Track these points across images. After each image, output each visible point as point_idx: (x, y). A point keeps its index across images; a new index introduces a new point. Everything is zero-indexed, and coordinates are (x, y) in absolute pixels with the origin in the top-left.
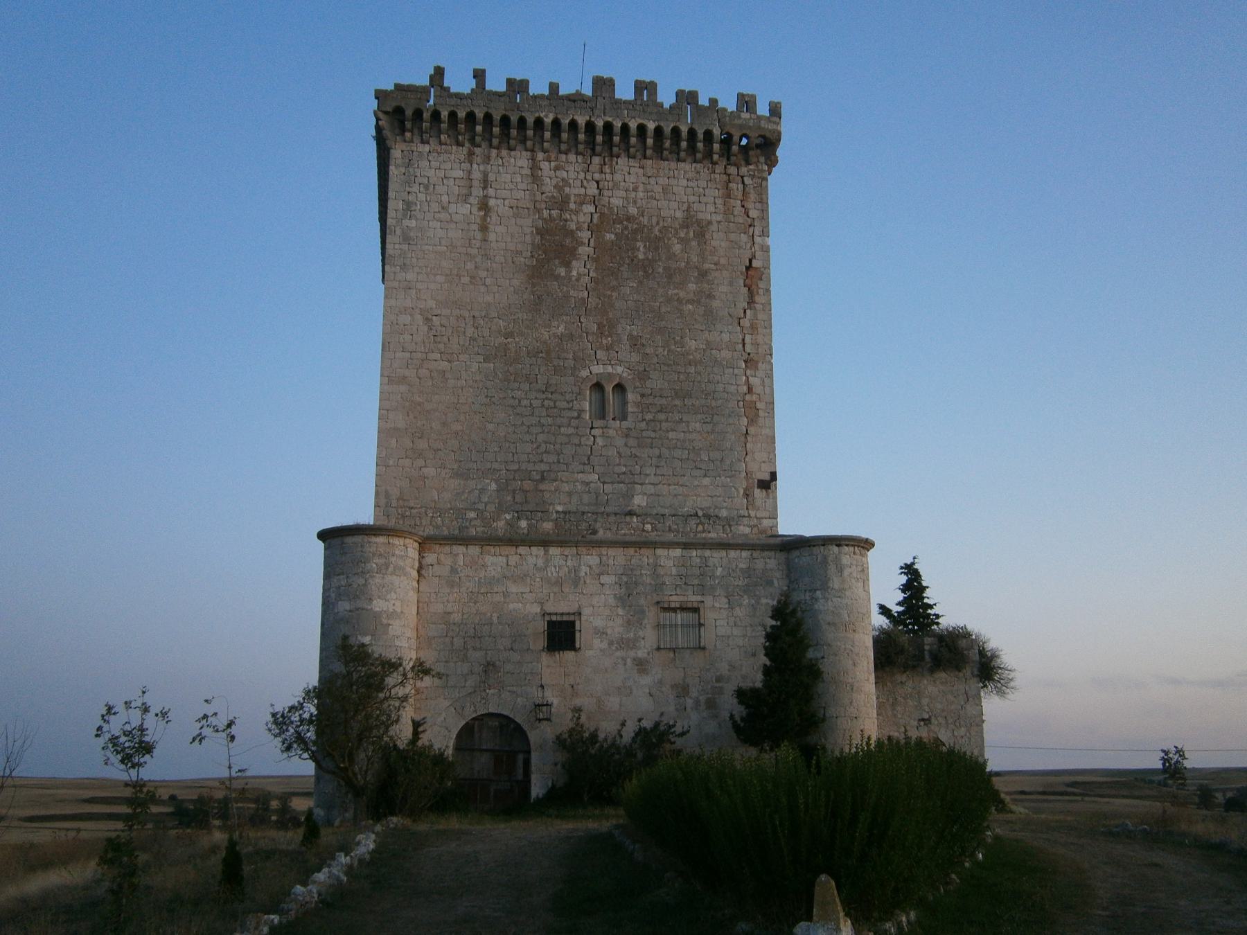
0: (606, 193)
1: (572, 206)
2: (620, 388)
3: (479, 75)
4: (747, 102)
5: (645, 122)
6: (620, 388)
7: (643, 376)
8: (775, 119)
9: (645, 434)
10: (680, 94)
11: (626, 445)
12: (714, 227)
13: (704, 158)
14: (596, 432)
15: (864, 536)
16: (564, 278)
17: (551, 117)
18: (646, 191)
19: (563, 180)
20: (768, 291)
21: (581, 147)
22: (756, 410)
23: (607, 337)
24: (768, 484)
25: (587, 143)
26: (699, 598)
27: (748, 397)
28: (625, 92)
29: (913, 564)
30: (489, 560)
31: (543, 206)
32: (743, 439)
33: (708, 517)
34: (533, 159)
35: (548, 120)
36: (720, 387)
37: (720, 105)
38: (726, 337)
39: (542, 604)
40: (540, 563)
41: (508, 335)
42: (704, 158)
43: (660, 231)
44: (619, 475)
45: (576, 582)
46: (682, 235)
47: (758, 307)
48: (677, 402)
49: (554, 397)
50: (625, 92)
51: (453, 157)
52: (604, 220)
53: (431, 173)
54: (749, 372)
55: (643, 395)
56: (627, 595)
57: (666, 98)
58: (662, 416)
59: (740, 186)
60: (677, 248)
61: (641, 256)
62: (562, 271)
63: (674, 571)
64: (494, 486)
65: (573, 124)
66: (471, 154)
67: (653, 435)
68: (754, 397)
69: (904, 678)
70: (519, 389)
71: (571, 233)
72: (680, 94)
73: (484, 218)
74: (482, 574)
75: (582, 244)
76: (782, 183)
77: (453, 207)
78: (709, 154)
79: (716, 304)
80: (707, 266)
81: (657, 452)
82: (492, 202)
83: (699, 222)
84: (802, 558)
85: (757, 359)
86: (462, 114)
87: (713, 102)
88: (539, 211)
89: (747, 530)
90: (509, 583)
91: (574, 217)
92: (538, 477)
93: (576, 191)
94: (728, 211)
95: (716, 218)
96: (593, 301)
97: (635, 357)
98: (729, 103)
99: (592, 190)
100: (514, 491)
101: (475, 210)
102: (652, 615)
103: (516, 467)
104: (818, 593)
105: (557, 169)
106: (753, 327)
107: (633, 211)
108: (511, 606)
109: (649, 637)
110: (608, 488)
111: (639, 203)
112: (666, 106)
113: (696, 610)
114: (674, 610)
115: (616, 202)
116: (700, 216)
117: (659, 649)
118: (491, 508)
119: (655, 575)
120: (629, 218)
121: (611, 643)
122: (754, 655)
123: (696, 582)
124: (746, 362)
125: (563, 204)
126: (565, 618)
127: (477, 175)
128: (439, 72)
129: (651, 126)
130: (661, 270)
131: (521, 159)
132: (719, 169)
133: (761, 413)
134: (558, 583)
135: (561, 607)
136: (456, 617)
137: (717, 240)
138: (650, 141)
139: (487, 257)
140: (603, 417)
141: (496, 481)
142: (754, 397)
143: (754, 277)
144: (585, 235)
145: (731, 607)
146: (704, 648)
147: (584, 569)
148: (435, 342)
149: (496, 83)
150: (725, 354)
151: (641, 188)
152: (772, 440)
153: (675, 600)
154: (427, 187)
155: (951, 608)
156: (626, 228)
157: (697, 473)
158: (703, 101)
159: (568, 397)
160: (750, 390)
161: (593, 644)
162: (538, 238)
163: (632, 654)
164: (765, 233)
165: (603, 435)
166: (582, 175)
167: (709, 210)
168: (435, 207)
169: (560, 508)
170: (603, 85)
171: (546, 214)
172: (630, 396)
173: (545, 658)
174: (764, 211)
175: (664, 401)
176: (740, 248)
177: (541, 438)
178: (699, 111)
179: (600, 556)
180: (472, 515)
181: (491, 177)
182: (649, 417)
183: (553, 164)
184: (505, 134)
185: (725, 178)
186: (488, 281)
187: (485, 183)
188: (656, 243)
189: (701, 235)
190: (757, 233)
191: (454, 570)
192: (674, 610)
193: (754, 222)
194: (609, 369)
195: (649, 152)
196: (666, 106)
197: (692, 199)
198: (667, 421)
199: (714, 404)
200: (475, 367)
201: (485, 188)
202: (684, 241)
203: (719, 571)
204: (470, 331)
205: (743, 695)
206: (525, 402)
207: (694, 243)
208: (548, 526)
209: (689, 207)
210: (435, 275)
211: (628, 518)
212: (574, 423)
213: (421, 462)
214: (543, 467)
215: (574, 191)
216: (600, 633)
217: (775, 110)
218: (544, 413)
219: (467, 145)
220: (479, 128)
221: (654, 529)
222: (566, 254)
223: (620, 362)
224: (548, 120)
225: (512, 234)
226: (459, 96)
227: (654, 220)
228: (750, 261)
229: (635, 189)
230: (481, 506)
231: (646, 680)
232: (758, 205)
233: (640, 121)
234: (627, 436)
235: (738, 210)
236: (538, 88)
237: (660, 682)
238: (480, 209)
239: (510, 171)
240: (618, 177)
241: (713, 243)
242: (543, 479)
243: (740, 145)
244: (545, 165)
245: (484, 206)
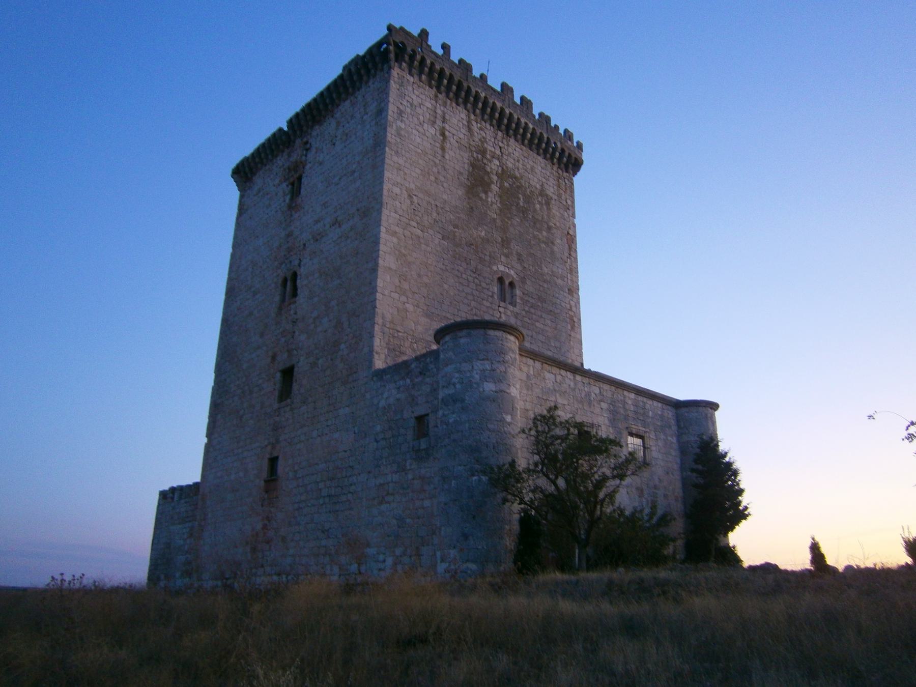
7: (523, 280)
62: (483, 196)
79: (555, 248)
144: (495, 178)
174: (573, 202)
175: (533, 301)
177: (473, 304)
179: (600, 388)
186: (445, 185)
188: (528, 199)
212: (490, 299)
244: (474, 123)
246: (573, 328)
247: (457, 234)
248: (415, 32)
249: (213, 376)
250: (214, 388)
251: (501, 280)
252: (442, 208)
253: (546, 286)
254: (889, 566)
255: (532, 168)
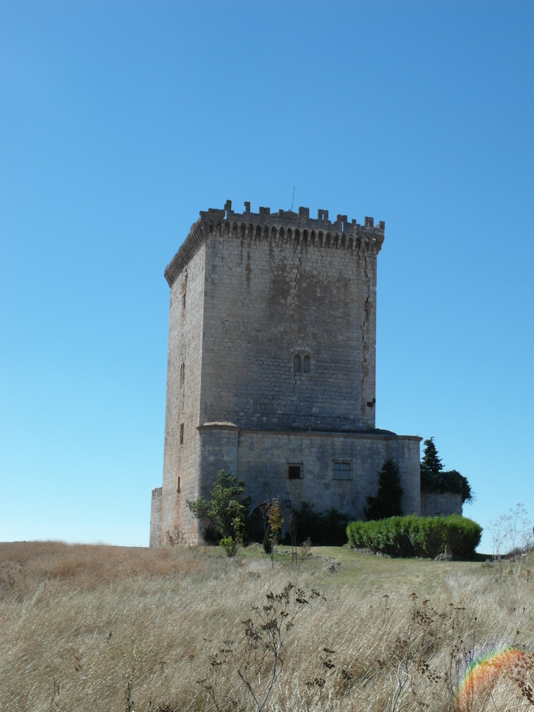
0: (303, 264)
1: (288, 270)
2: (307, 357)
3: (247, 205)
4: (369, 221)
5: (322, 230)
6: (307, 357)
7: (318, 352)
8: (381, 230)
9: (318, 379)
10: (339, 216)
11: (310, 384)
12: (351, 282)
13: (348, 248)
14: (297, 378)
15: (420, 436)
16: (284, 304)
17: (280, 226)
18: (322, 263)
19: (284, 257)
20: (375, 314)
21: (293, 242)
22: (367, 370)
23: (302, 333)
24: (372, 404)
25: (295, 239)
26: (350, 459)
27: (364, 364)
28: (314, 215)
29: (431, 440)
30: (266, 440)
31: (275, 269)
32: (361, 383)
33: (344, 418)
34: (270, 246)
35: (278, 228)
36: (352, 359)
37: (357, 223)
38: (355, 335)
39: (287, 459)
40: (286, 442)
41: (259, 331)
42: (348, 248)
43: (327, 283)
44: (306, 398)
45: (301, 450)
46: (337, 285)
47: (370, 321)
48: (333, 365)
49: (278, 361)
50: (314, 215)
51: (234, 244)
52: (302, 277)
53: (224, 252)
54: (365, 352)
55: (318, 361)
56: (321, 457)
57: (333, 218)
58: (326, 372)
59: (364, 262)
60: (335, 291)
61: (318, 295)
62: (283, 301)
63: (340, 447)
64: (252, 401)
65: (290, 231)
66: (242, 243)
67: (322, 380)
68: (367, 364)
69: (430, 495)
70: (263, 357)
71: (287, 283)
72: (339, 216)
73: (248, 274)
74: (263, 446)
75: (292, 288)
76: (383, 257)
77: (234, 268)
78: (351, 246)
79: (351, 319)
80: (348, 300)
81: (323, 388)
82: (252, 267)
83: (345, 279)
84: (393, 444)
85: (368, 346)
86: (239, 224)
87: (354, 221)
88: (273, 272)
89: (361, 425)
90: (274, 450)
91: (289, 275)
92: (271, 398)
93: (289, 262)
94: (359, 274)
95: (354, 277)
96: (296, 316)
97: (315, 343)
98: (361, 222)
99: (297, 262)
100: (260, 404)
101: (244, 271)
102: (331, 465)
103: (261, 393)
104: (400, 459)
105: (281, 251)
106: (368, 330)
107: (315, 273)
108: (275, 460)
109: (330, 474)
110: (301, 403)
111: (318, 270)
112: (332, 222)
113: (348, 464)
114: (340, 464)
115: (308, 268)
116: (345, 276)
117: (334, 479)
118: (251, 411)
119: (333, 449)
120: (313, 276)
121: (314, 476)
122: (372, 483)
123: (349, 452)
124: (364, 347)
125: (283, 268)
126: (296, 465)
127: (245, 254)
128: (229, 203)
129: (325, 232)
130: (327, 302)
131: (264, 246)
132: (355, 253)
133: (370, 371)
134: (294, 451)
135: (295, 460)
136: (253, 464)
137: (353, 288)
138: (324, 240)
139: (249, 293)
140: (300, 371)
141: (253, 399)
142: (367, 364)
143: (369, 307)
144: (293, 284)
145: (363, 463)
146: (352, 480)
147: (304, 445)
148: (226, 333)
149: (254, 209)
150: (355, 343)
151: (319, 262)
152: (374, 384)
153: (341, 459)
154: (222, 258)
155: (448, 464)
156: (312, 281)
157: (340, 398)
158: (349, 221)
159: (285, 361)
160: (365, 360)
161: (308, 478)
162: (272, 285)
163: (323, 481)
164: (375, 285)
165: (300, 380)
166: (292, 255)
167: (350, 273)
168: (226, 268)
169: (280, 412)
170: (304, 211)
171: (276, 273)
172: (312, 362)
173: (288, 481)
174: (375, 274)
175: (326, 364)
176: (363, 292)
177: (273, 379)
178: (347, 225)
179: (311, 440)
180: (243, 414)
181: (251, 255)
182: (320, 371)
183: (280, 249)
184: (259, 234)
185: (357, 257)
186: (250, 305)
187: (249, 258)
188: (325, 289)
189: (346, 285)
190: (371, 285)
191: (252, 444)
192: (340, 464)
193: (370, 280)
194: (303, 348)
195: (323, 245)
196: (332, 222)
197: (342, 268)
198: (328, 373)
199: (349, 366)
200: (244, 346)
201: (249, 260)
202: (338, 288)
203: (359, 448)
204: (242, 329)
205: (370, 500)
206: (265, 363)
207: (342, 289)
208: (275, 420)
209: (341, 272)
210: (226, 301)
211: (310, 418)
212: (287, 373)
213: (219, 389)
214: (274, 393)
215: (289, 262)
216: (310, 472)
217: (382, 225)
218: (274, 368)
219: (241, 238)
220: (247, 232)
221: (321, 423)
222: (285, 293)
223: (308, 346)
224: (278, 228)
225: (261, 283)
226: (238, 215)
227: (325, 278)
228: (367, 298)
229: (317, 262)
230: (246, 410)
231: (328, 492)
232: (372, 271)
233: (320, 230)
234: (310, 380)
235: (363, 274)
236: (274, 210)
237: (334, 493)
238: (246, 270)
239: (260, 250)
240: (309, 256)
241: (351, 289)
242: (273, 398)
243: (364, 241)
244: (275, 249)
245: (248, 269)
246: (366, 374)
247: (259, 336)
248: (221, 207)
249: (11, 540)
250: (9, 543)
251: (298, 357)
252: (247, 322)
253: (340, 350)
254: (43, 541)
255: (331, 263)
